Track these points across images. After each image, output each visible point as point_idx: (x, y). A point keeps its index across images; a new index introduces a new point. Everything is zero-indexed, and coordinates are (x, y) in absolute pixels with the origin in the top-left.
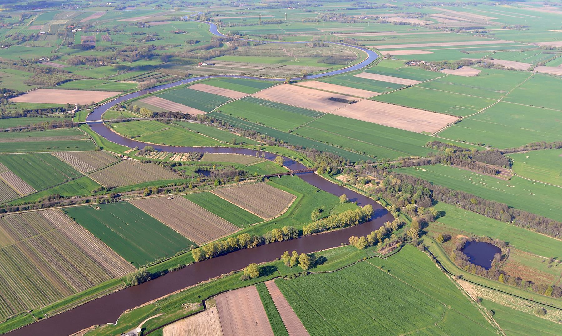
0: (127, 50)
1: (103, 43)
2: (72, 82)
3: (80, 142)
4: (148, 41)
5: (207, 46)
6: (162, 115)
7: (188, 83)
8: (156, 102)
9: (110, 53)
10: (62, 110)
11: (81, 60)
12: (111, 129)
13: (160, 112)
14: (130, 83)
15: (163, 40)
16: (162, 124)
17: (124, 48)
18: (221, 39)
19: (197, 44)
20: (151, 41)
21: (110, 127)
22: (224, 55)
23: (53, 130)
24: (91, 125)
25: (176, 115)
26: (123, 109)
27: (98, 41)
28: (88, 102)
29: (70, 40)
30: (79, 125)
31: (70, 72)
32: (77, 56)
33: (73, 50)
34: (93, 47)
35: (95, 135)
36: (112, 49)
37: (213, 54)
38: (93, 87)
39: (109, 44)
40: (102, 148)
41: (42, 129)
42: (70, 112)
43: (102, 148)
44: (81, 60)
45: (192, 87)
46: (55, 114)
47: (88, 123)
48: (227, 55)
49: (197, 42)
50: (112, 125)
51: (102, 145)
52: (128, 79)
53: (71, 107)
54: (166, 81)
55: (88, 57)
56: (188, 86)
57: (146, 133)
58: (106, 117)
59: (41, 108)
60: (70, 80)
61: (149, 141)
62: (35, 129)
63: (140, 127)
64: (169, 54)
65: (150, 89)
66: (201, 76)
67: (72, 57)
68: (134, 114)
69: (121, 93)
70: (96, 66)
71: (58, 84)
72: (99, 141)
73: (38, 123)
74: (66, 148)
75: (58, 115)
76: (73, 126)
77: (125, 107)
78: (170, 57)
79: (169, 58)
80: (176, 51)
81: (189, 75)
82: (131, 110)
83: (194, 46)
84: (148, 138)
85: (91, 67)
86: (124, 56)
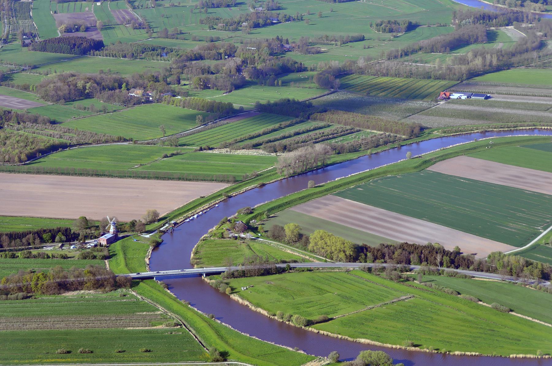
0: (205, 53)
1: (123, 34)
2: (68, 152)
3: (153, 336)
4: (257, 25)
5: (449, 38)
6: (381, 254)
7: (426, 155)
8: (339, 214)
9: (158, 65)
10: (70, 237)
11: (80, 84)
13: (374, 244)
14: (238, 151)
15: (301, 23)
16: (388, 283)
17: (195, 47)
18: (485, 18)
19: (412, 34)
20: (265, 25)
21: (228, 291)
22: (509, 66)
23: (59, 297)
24: (170, 283)
25: (427, 254)
26: (250, 235)
28: (139, 212)
29: (23, 24)
30: (134, 283)
31: (53, 123)
32: (68, 72)
33: (40, 56)
34: (98, 46)
35: (189, 314)
36: (159, 51)
37: (478, 63)
38: (136, 168)
39: (142, 37)
40: (224, 356)
41: (27, 293)
42: (91, 243)
43: (224, 356)
44: (80, 84)
46: (49, 249)
47: (160, 278)
48: (519, 64)
49: (411, 27)
50: (234, 283)
51: (222, 347)
52: (236, 144)
53: (92, 228)
54: (354, 150)
55: (97, 75)
56: (427, 163)
57: (346, 312)
59: (8, 231)
60: (64, 147)
61: (364, 335)
63: (321, 291)
64: (336, 64)
65: (313, 172)
66: (460, 133)
70: (128, 102)
71: (32, 157)
72: (213, 336)
73: (13, 274)
74: (114, 352)
76: (117, 284)
77: (255, 230)
78: (341, 73)
79: (337, 78)
80: (356, 55)
81: (422, 129)
82: (277, 235)
83: (406, 41)
84: (359, 323)
85: (111, 106)
86: (203, 71)
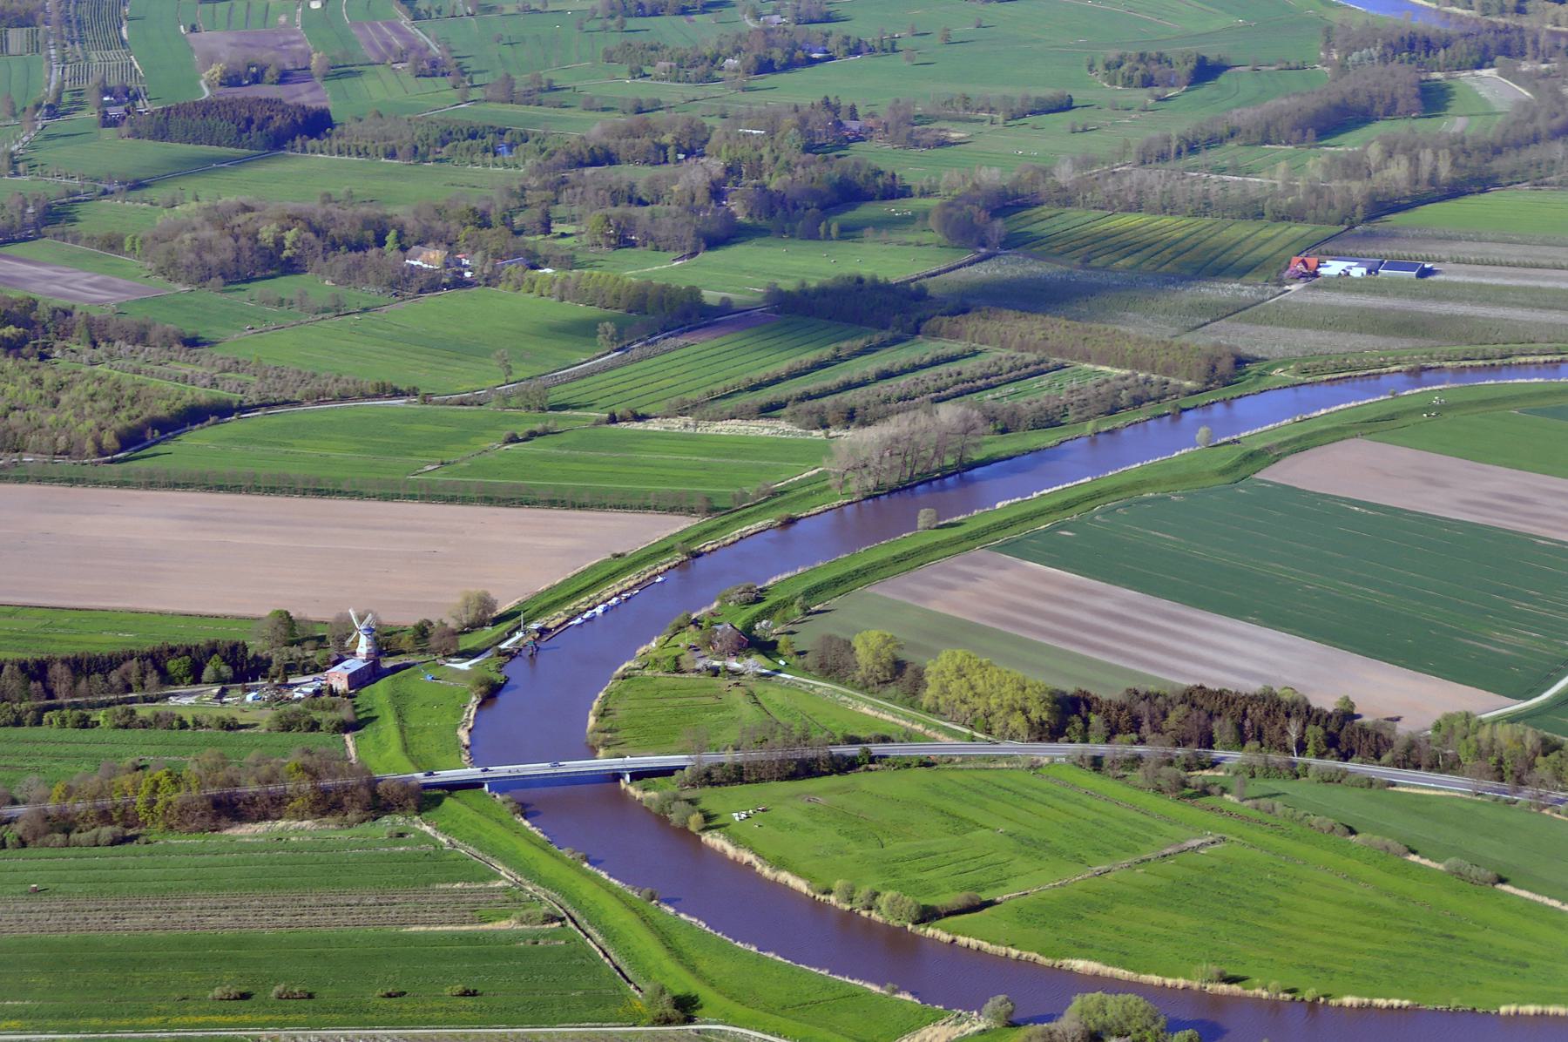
0: (621, 146)
2: (233, 425)
3: (483, 951)
4: (766, 67)
6: (1130, 718)
7: (1254, 436)
9: (486, 179)
10: (244, 668)
11: (267, 234)
12: (709, 839)
13: (1109, 691)
14: (715, 424)
15: (897, 61)
17: (592, 129)
18: (1417, 46)
19: (1206, 90)
20: (790, 65)
22: (1484, 183)
23: (214, 840)
24: (529, 800)
25: (1260, 719)
26: (754, 664)
27: (339, 71)
29: (103, 63)
30: (428, 799)
31: (192, 342)
32: (231, 198)
34: (317, 124)
35: (586, 890)
37: (1397, 173)
39: (439, 100)
40: (686, 1008)
41: (124, 827)
42: (304, 686)
43: (686, 1008)
44: (267, 234)
45: (1296, 472)
46: (185, 701)
47: (500, 785)
48: (1514, 179)
49: (1205, 71)
50: (711, 799)
51: (682, 983)
53: (306, 643)
54: (1048, 421)
55: (313, 206)
58: (648, 720)
59: (68, 650)
60: (223, 411)
61: (1083, 948)
62: (64, 825)
63: (959, 824)
64: (992, 176)
65: (929, 484)
66: (1351, 374)
67: (192, 205)
68: (872, 712)
69: (681, 524)
70: (404, 284)
71: (133, 440)
73: (84, 774)
74: (374, 997)
75: (219, 711)
76: (378, 802)
77: (768, 648)
78: (1008, 203)
81: (1240, 362)
83: (1189, 112)
84: (1067, 917)
85: (357, 295)
86: (616, 197)
